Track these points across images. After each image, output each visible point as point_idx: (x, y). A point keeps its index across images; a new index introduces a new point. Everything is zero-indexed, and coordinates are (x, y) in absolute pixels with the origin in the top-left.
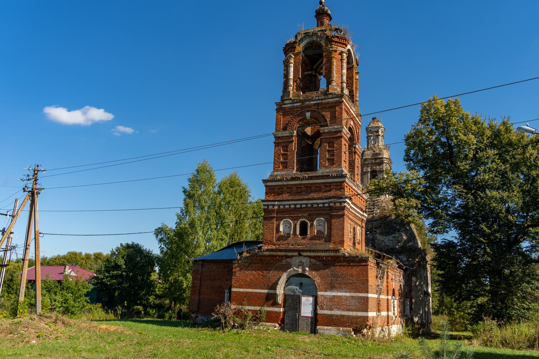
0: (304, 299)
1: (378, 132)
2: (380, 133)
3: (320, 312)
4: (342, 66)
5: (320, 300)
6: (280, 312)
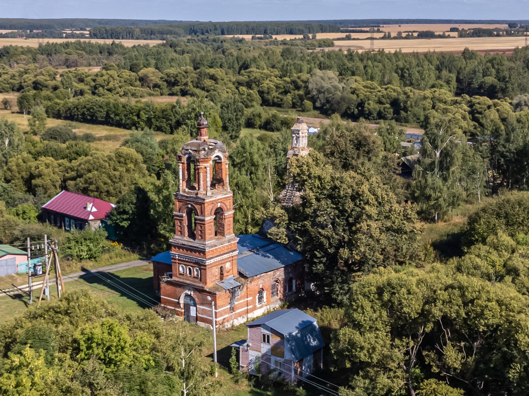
0: (191, 308)
1: (298, 134)
3: (198, 315)
5: (198, 309)
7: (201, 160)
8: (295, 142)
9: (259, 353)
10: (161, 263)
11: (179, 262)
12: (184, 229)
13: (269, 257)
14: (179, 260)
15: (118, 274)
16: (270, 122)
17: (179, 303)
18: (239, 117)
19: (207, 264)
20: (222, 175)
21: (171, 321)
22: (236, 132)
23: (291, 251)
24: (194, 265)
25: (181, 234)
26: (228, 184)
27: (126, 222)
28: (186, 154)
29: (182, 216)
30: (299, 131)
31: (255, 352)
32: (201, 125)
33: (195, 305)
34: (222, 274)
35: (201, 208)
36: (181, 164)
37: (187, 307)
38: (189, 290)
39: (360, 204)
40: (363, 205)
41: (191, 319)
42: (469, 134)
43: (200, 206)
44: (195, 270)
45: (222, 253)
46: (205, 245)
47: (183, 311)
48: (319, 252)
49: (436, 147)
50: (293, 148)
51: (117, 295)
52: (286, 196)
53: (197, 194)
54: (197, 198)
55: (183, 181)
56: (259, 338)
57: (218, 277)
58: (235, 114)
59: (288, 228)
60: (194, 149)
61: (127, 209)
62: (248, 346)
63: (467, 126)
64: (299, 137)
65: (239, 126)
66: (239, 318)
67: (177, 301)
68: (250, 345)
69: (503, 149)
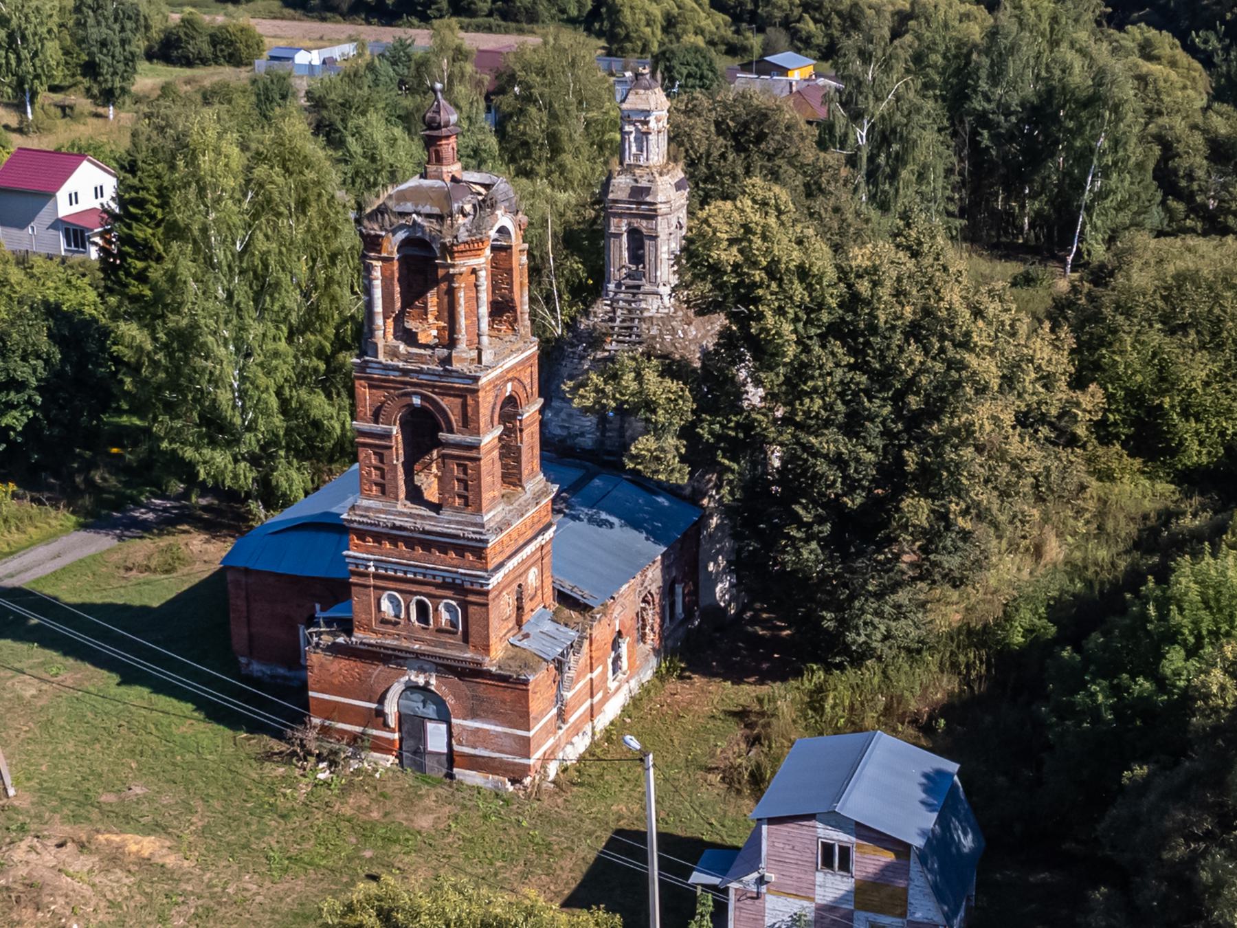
0: (430, 726)
1: (646, 123)
2: (653, 124)
3: (456, 748)
4: (477, 298)
5: (455, 731)
6: (394, 740)
7: (462, 247)
8: (634, 150)
9: (806, 903)
10: (258, 572)
11: (380, 583)
12: (395, 478)
13: (612, 525)
14: (377, 576)
15: (48, 591)
16: (179, 39)
17: (380, 714)
18: (129, 34)
19: (490, 587)
20: (511, 291)
21: (358, 772)
22: (123, 79)
23: (658, 494)
24: (439, 592)
25: (383, 492)
26: (527, 316)
27: (17, 414)
28: (401, 227)
29: (387, 436)
30: (648, 113)
31: (791, 900)
32: (439, 127)
33: (444, 716)
34: (520, 608)
35: (464, 406)
36: (378, 264)
37: (412, 727)
38: (422, 670)
39: (942, 350)
40: (951, 352)
41: (429, 762)
42: (723, 48)
43: (459, 401)
44: (441, 608)
45: (521, 542)
46: (482, 526)
47: (396, 736)
48: (805, 508)
49: (856, 116)
50: (629, 169)
51: (107, 680)
52: (612, 320)
53: (447, 361)
54: (449, 373)
55: (385, 318)
56: (808, 856)
57: (512, 623)
58: (117, 27)
59: (687, 432)
60: (427, 209)
61: (19, 375)
62: (761, 881)
63: (713, 28)
64: (647, 133)
65: (130, 60)
66: (575, 739)
67: (374, 706)
68: (771, 876)
69: (986, 105)
